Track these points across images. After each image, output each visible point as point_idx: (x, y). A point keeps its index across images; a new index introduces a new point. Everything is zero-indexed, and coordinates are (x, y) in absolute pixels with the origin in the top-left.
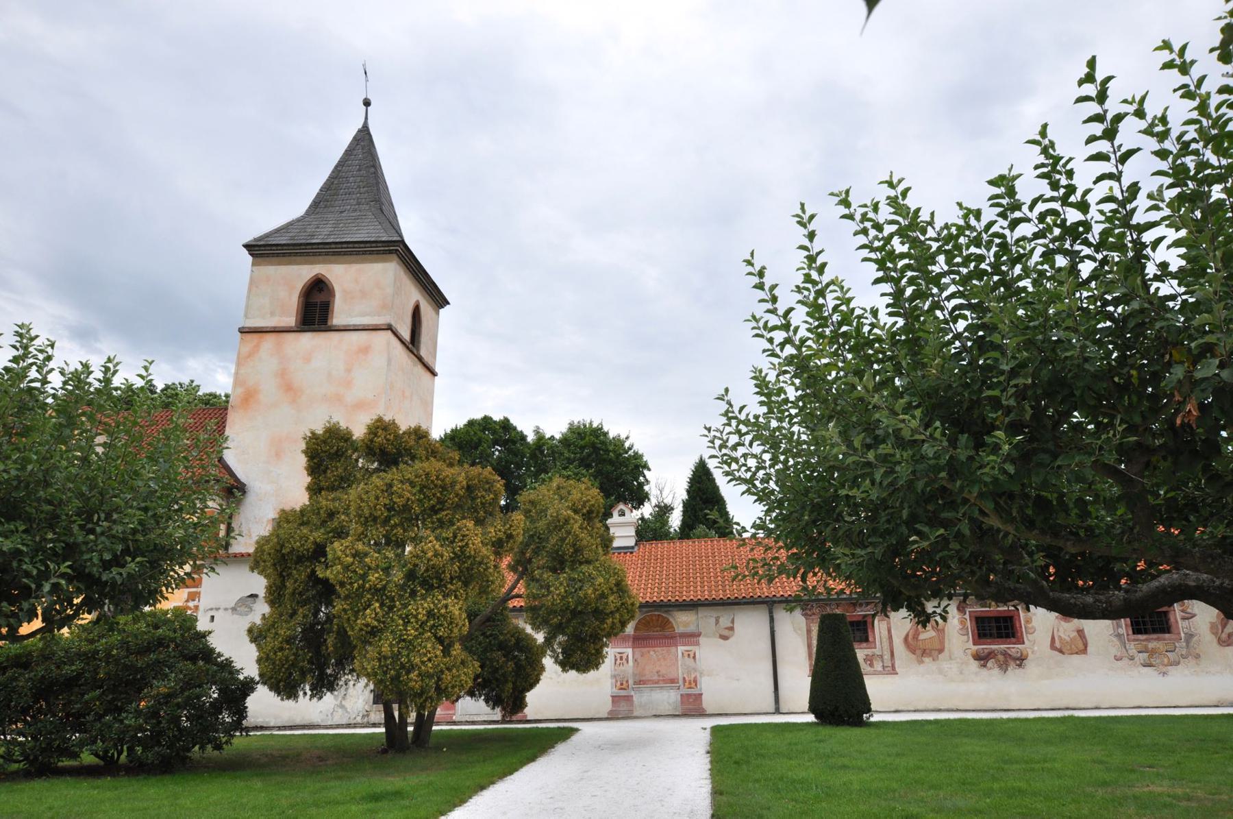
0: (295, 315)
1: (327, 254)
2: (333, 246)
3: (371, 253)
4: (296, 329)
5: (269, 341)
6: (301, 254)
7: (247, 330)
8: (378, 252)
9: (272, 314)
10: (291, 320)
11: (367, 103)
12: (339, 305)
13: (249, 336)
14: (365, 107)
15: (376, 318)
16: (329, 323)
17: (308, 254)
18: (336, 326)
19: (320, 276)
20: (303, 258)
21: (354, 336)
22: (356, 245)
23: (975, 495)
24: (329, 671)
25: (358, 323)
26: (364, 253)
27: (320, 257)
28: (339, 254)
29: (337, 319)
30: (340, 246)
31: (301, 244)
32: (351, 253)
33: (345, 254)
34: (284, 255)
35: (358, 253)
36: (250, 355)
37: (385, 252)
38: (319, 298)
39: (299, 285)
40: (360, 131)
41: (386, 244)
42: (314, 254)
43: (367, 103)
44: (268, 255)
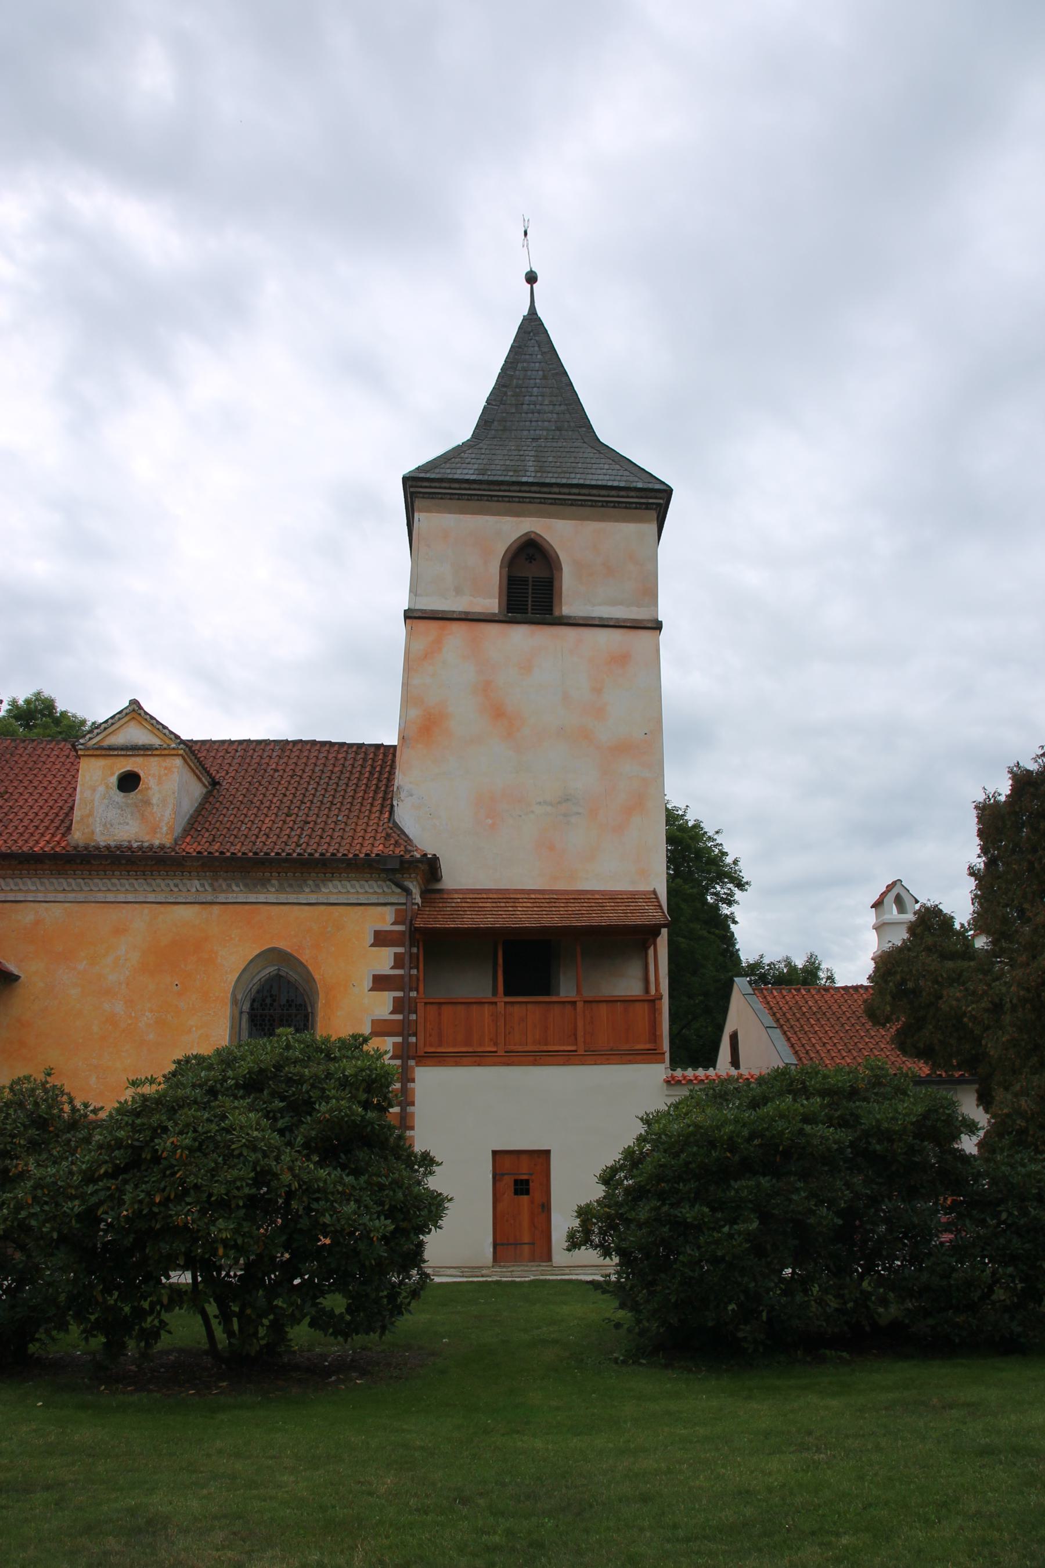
0: (497, 594)
1: (543, 501)
2: (556, 490)
3: (616, 505)
4: (502, 618)
5: (458, 633)
6: (500, 499)
7: (419, 614)
8: (628, 506)
9: (458, 591)
10: (492, 604)
11: (531, 278)
12: (569, 582)
13: (422, 625)
14: (529, 286)
15: (634, 609)
16: (556, 613)
17: (510, 500)
18: (570, 617)
19: (533, 536)
20: (502, 504)
21: (603, 635)
22: (594, 492)
23: (81, 1136)
24: (779, 1201)
25: (605, 616)
26: (605, 504)
27: (531, 507)
28: (563, 502)
29: (569, 606)
30: (566, 490)
31: (502, 483)
32: (582, 504)
33: (573, 503)
34: (470, 497)
35: (594, 504)
36: (427, 655)
37: (639, 506)
38: (532, 571)
39: (500, 549)
40: (525, 319)
41: (642, 494)
42: (521, 500)
43: (531, 278)
44: (442, 496)
